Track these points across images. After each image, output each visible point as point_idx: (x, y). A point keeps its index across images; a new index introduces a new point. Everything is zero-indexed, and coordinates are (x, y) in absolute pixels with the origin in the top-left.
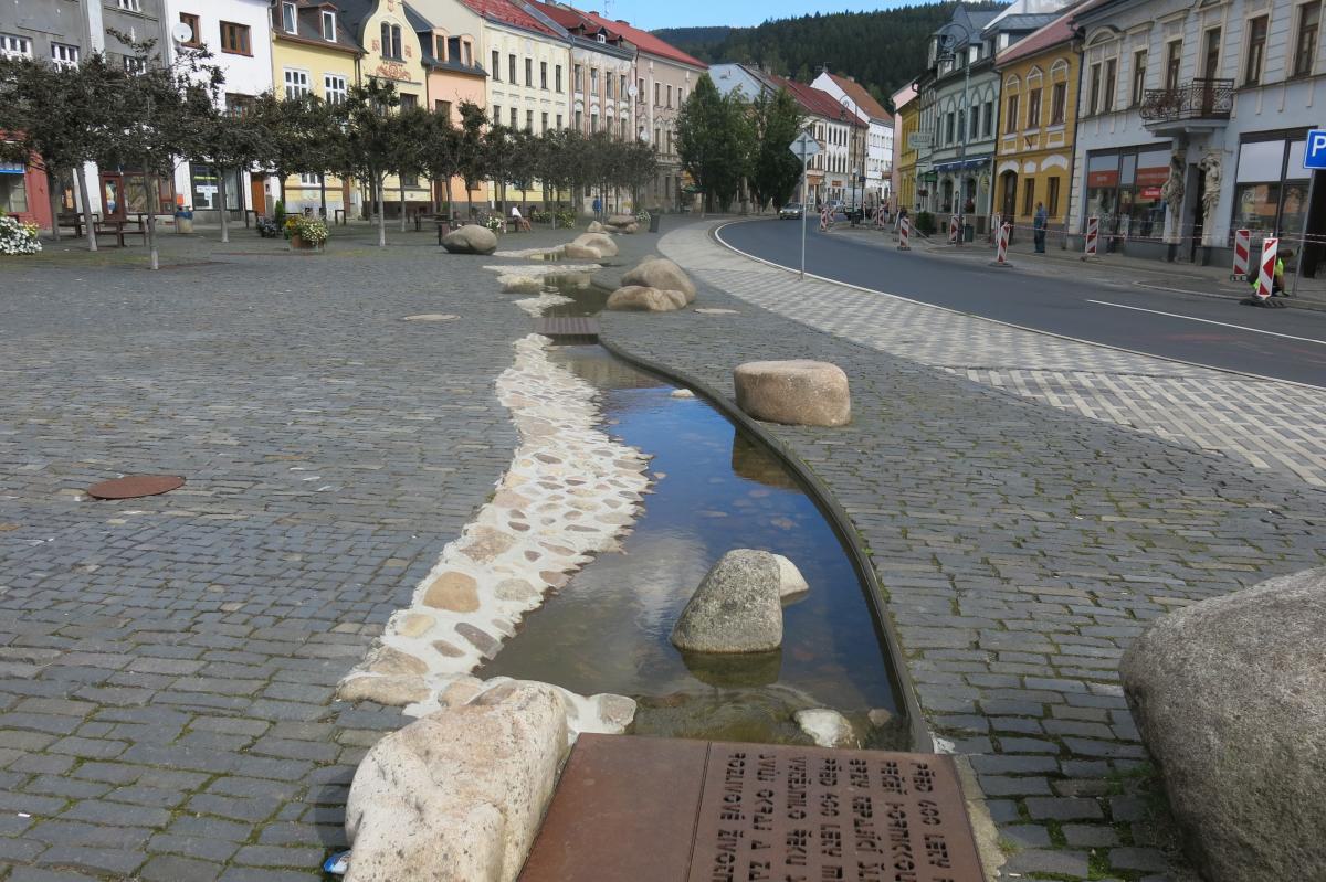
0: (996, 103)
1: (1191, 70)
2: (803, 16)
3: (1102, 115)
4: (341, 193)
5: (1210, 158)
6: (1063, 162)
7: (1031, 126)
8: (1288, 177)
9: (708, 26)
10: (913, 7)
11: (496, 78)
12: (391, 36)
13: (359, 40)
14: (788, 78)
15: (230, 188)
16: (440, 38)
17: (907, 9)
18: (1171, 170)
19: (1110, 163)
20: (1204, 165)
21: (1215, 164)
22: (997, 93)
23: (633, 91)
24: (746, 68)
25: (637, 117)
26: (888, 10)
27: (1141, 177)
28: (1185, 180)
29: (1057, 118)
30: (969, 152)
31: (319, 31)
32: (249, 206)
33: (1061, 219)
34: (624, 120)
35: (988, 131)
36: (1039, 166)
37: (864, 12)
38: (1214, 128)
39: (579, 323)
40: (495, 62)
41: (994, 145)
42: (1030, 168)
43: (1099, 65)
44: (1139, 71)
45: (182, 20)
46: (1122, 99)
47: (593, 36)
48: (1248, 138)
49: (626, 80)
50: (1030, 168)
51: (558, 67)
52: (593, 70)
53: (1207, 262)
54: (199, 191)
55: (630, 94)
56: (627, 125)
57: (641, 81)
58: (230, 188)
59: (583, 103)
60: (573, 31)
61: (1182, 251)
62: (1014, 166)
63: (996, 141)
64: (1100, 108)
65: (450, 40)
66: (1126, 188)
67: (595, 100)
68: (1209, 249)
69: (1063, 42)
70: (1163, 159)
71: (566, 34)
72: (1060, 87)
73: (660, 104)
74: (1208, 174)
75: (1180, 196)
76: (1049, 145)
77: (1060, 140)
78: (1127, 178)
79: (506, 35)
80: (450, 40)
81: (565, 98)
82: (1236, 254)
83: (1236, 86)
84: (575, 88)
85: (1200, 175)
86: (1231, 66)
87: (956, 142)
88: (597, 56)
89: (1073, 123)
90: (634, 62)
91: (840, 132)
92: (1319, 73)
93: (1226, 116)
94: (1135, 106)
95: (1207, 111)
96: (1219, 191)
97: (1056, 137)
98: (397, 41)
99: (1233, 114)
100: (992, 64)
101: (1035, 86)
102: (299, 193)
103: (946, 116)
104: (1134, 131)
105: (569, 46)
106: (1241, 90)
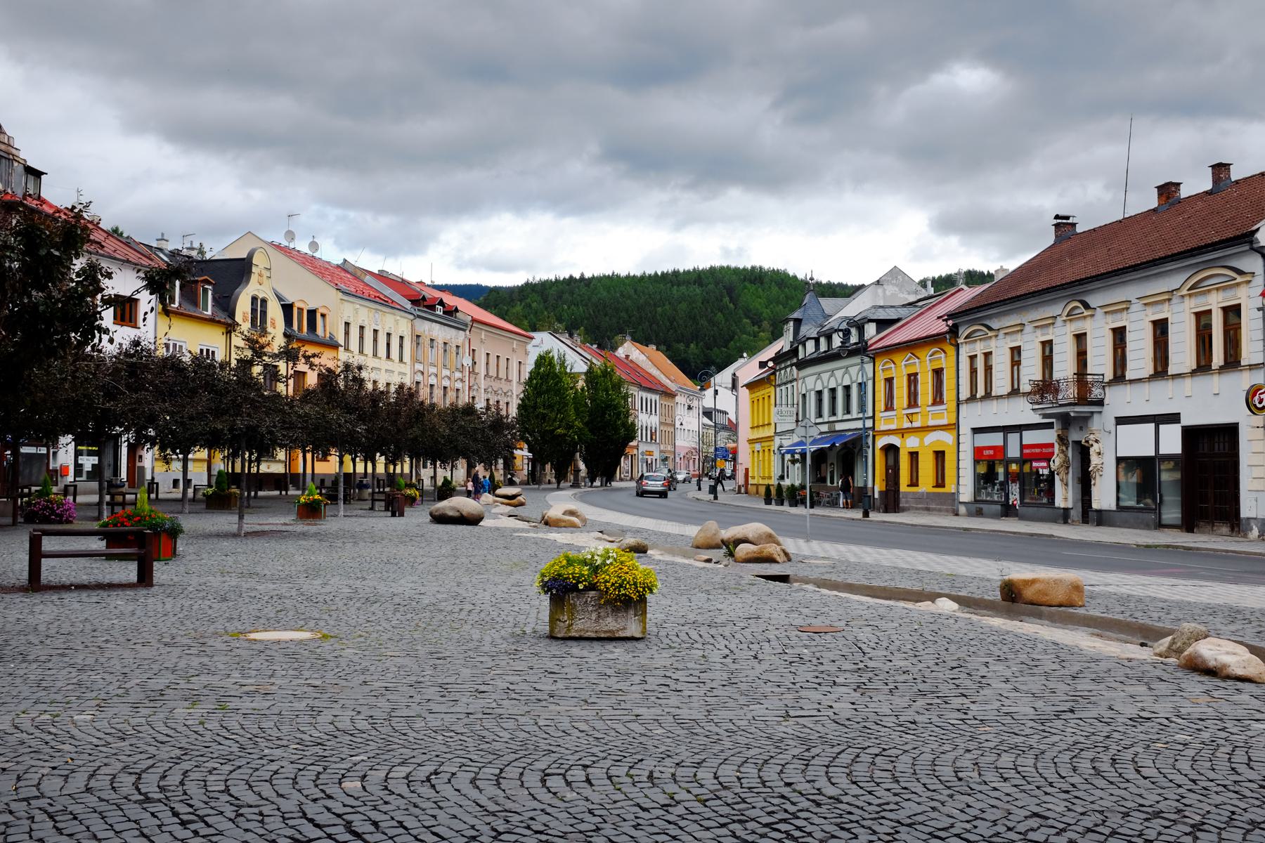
0: (870, 384)
1: (1064, 368)
2: (567, 277)
3: (983, 398)
5: (1092, 436)
6: (947, 438)
7: (910, 406)
8: (1160, 453)
9: (468, 283)
10: (681, 271)
14: (595, 346)
15: (109, 459)
16: (300, 310)
17: (676, 273)
18: (1056, 446)
19: (996, 439)
20: (1087, 442)
21: (1097, 441)
22: (871, 375)
23: (467, 361)
24: (557, 335)
25: (470, 387)
26: (656, 273)
27: (1026, 451)
28: (1070, 454)
29: (938, 399)
30: (839, 427)
31: (196, 304)
32: (124, 475)
33: (950, 487)
34: (458, 390)
35: (862, 408)
36: (922, 440)
37: (632, 274)
38: (1092, 413)
40: (347, 333)
41: (871, 420)
42: (911, 443)
43: (976, 356)
44: (1016, 363)
46: (1001, 384)
47: (432, 308)
48: (1121, 421)
49: (461, 350)
50: (911, 443)
51: (402, 338)
52: (432, 340)
53: (1100, 523)
54: (80, 462)
55: (465, 364)
57: (474, 350)
58: (109, 459)
60: (415, 302)
61: (1076, 514)
62: (894, 440)
63: (873, 417)
64: (981, 392)
65: (309, 312)
66: (1014, 460)
67: (432, 370)
68: (1099, 512)
69: (938, 335)
70: (1049, 436)
71: (408, 305)
72: (938, 373)
73: (490, 374)
74: (1092, 450)
75: (1068, 468)
76: (931, 423)
77: (943, 418)
78: (1014, 451)
79: (358, 306)
80: (309, 312)
81: (406, 369)
82: (768, 530)
83: (1106, 380)
84: (415, 360)
85: (1084, 452)
86: (1100, 362)
87: (826, 417)
88: (436, 326)
89: (955, 404)
90: (468, 332)
92: (1174, 373)
93: (1100, 403)
94: (1015, 392)
95: (1082, 399)
96: (1102, 464)
98: (264, 313)
99: (1106, 402)
101: (912, 371)
103: (813, 393)
104: (1021, 411)
105: (412, 317)
106: (1110, 383)
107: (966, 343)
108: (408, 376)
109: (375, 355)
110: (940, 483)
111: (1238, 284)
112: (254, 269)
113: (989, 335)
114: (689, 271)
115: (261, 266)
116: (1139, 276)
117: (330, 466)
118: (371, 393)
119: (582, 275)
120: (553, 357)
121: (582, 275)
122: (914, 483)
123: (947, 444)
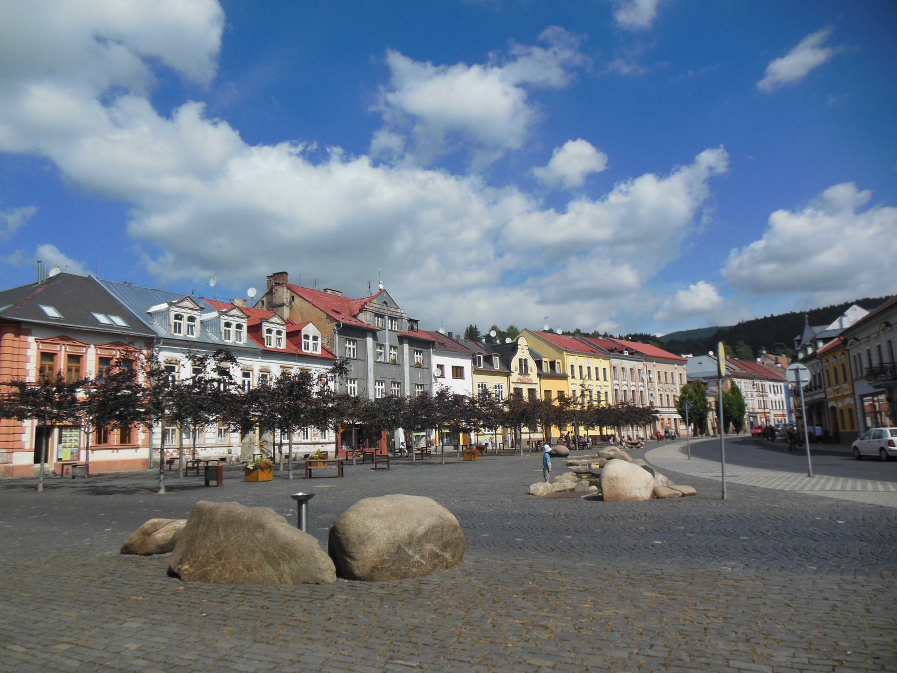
4: (501, 436)
11: (573, 377)
12: (523, 363)
13: (508, 366)
34: (641, 392)
39: (378, 321)
41: (667, 406)
42: (840, 405)
45: (438, 367)
47: (622, 352)
49: (642, 371)
52: (623, 368)
56: (644, 394)
59: (627, 386)
81: (608, 383)
91: (781, 387)
97: (846, 390)
98: (526, 366)
100: (815, 355)
102: (484, 437)
108: (610, 386)
109: (598, 379)
110: (853, 427)
112: (519, 347)
114: (827, 308)
115: (523, 345)
117: (595, 432)
119: (772, 315)
121: (772, 315)
122: (844, 427)
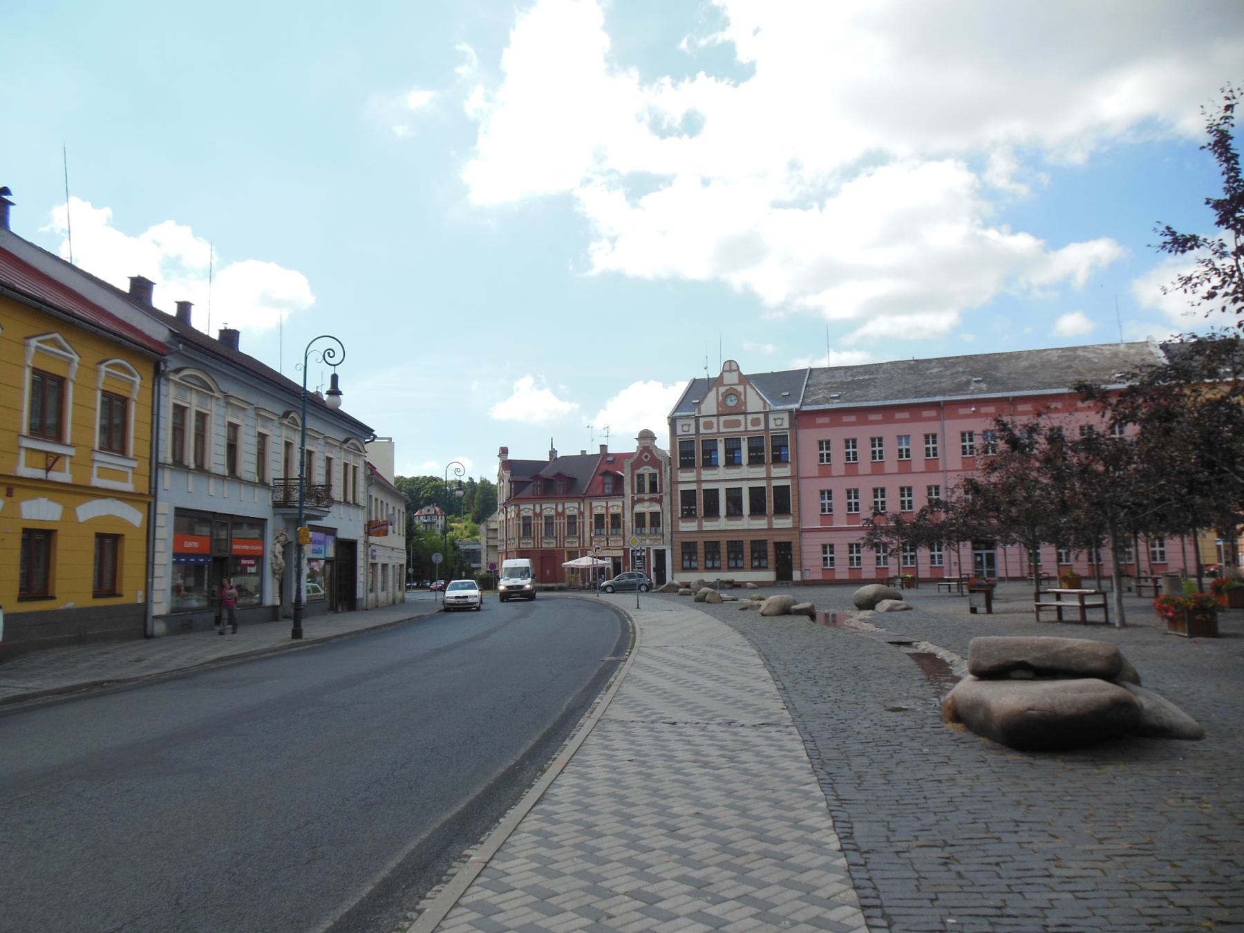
6: (134, 516)
33: (132, 593)
107: (287, 426)
111: (212, 397)
113: (216, 395)
116: (279, 396)
118: (914, 525)
120: (949, 690)
123: (132, 526)
